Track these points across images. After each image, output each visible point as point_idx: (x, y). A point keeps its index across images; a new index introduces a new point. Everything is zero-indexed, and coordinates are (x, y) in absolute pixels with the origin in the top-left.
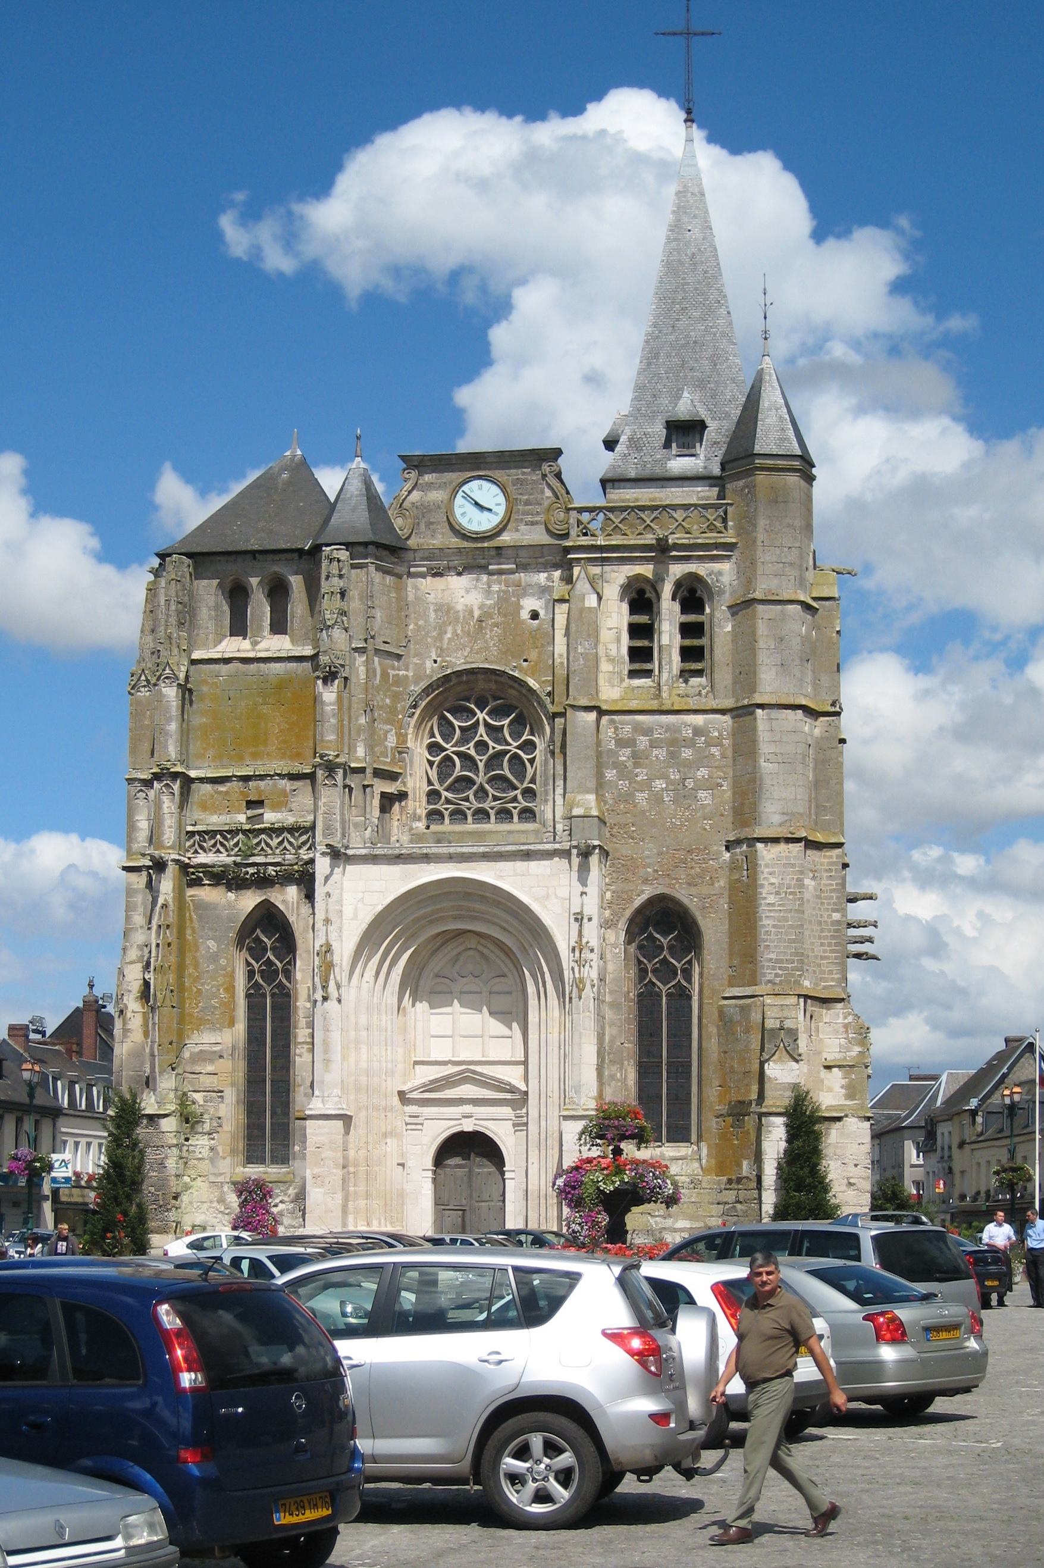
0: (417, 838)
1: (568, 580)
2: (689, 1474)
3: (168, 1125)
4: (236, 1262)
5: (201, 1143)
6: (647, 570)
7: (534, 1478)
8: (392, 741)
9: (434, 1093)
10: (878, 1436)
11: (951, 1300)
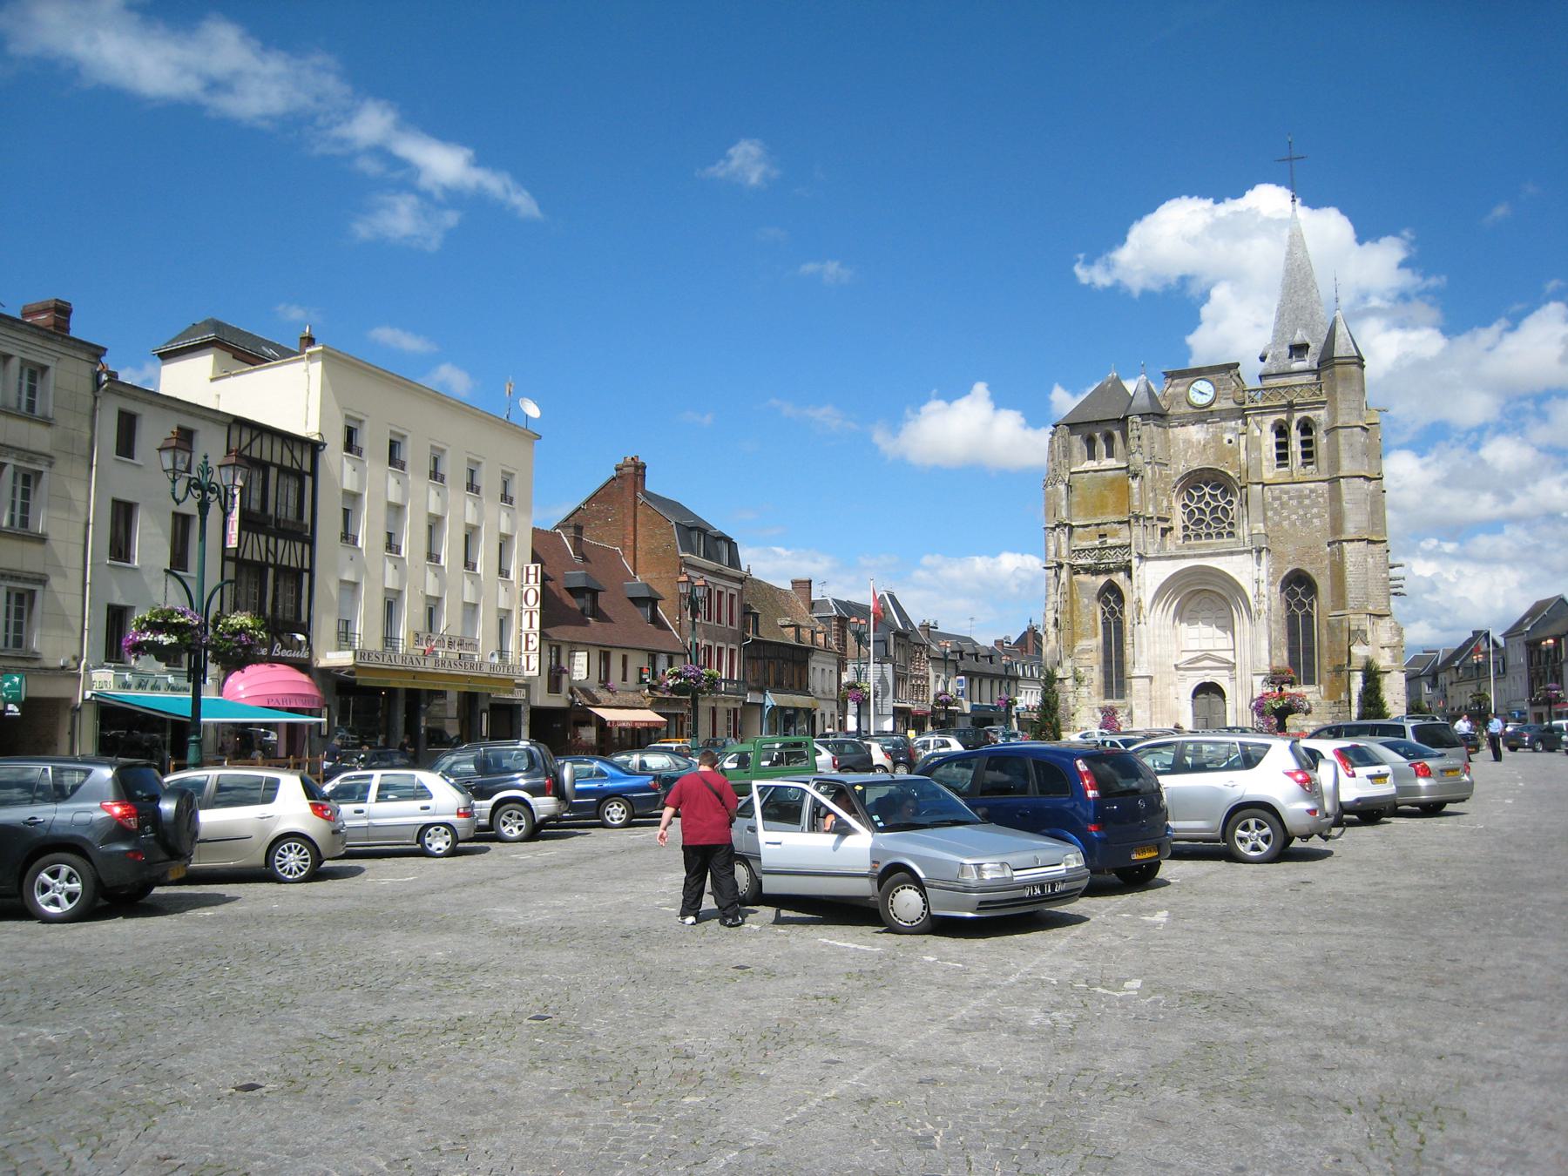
0: (1179, 548)
1: (1246, 424)
2: (1326, 838)
3: (1069, 682)
4: (1104, 743)
5: (1083, 690)
6: (1284, 417)
7: (1251, 839)
8: (1165, 503)
9: (1192, 665)
10: (1418, 822)
11: (1453, 757)
